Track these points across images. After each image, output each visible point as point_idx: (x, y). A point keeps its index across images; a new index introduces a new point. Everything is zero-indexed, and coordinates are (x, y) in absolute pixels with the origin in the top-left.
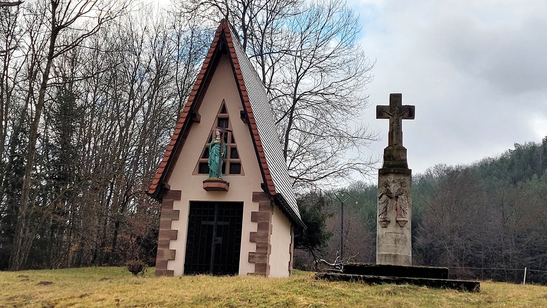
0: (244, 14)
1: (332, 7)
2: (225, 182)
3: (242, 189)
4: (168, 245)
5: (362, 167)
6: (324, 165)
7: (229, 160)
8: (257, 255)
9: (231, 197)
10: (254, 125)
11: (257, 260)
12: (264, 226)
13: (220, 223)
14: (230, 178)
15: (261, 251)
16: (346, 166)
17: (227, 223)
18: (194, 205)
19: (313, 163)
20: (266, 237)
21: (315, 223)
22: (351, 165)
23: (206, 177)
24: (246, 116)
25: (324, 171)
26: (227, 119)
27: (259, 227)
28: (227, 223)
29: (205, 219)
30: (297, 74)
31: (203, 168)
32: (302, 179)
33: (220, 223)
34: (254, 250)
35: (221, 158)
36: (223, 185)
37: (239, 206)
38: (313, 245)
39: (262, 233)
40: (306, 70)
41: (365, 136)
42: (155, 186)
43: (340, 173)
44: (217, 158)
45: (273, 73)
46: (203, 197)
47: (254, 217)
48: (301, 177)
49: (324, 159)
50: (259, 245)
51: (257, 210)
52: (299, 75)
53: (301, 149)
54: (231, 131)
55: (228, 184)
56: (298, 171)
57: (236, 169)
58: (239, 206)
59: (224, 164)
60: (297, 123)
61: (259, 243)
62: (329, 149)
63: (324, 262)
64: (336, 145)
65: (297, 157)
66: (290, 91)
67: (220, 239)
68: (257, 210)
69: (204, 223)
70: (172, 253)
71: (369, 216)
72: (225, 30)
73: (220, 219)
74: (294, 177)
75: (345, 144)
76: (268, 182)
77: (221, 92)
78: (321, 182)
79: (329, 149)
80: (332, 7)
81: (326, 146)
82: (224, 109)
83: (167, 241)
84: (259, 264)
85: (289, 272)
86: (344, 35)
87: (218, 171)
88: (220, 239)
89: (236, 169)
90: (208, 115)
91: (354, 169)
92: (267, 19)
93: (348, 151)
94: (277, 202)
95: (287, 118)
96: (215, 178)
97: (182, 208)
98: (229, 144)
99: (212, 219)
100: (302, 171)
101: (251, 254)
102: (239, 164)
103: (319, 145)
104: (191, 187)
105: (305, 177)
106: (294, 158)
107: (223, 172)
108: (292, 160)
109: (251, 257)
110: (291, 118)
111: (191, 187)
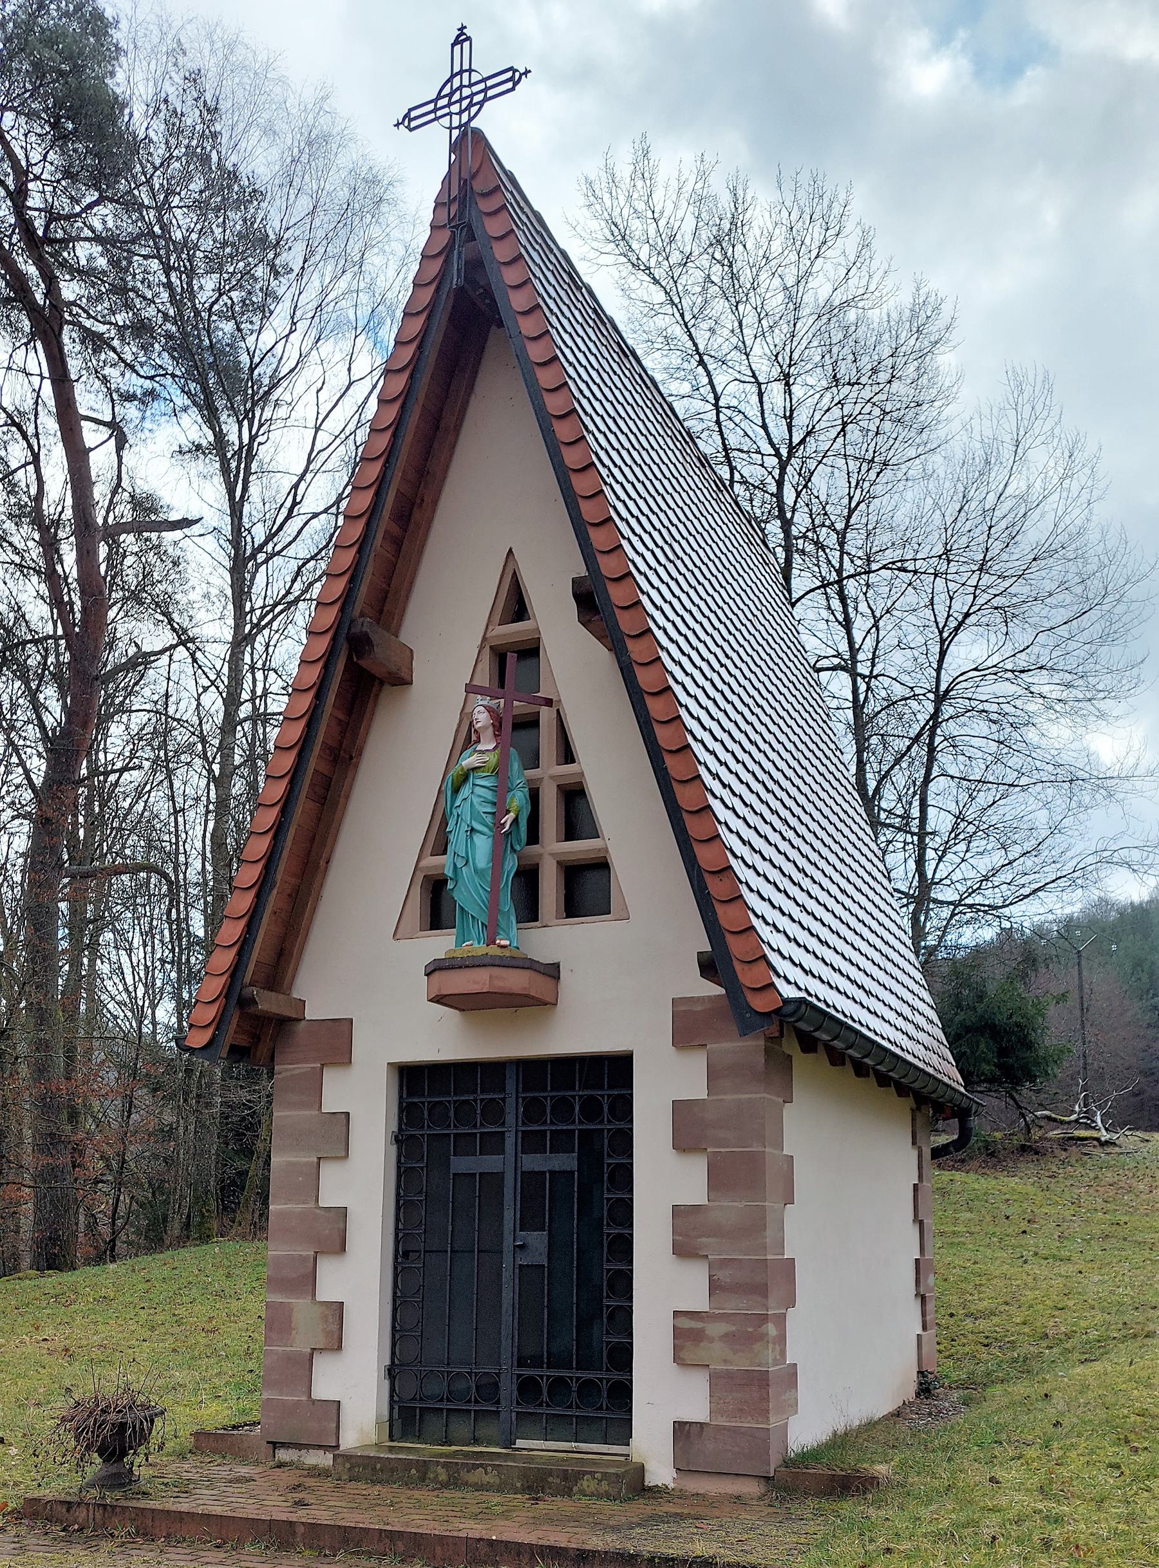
0: (780, 484)
1: (1022, 433)
2: (530, 965)
3: (616, 987)
4: (309, 1281)
5: (1136, 855)
6: (1029, 862)
7: (554, 848)
8: (716, 1329)
9: (572, 1034)
10: (646, 641)
11: (716, 1353)
12: (745, 1172)
13: (533, 1162)
14: (557, 939)
15: (733, 1305)
16: (1091, 859)
17: (567, 1162)
18: (413, 1079)
19: (998, 858)
20: (758, 1227)
21: (1018, 1025)
22: (1105, 854)
23: (441, 944)
24: (599, 603)
25: (1032, 877)
26: (530, 651)
27: (717, 1180)
28: (567, 1162)
29: (464, 1144)
30: (941, 633)
31: (436, 903)
32: (970, 906)
33: (533, 1162)
34: (700, 1302)
35: (502, 841)
36: (515, 981)
37: (617, 1068)
38: (1016, 1082)
39: (732, 1208)
40: (963, 622)
41: (1141, 771)
42: (211, 1013)
43: (1073, 878)
44: (483, 845)
45: (878, 642)
46: (442, 1039)
47: (689, 1128)
48: (969, 901)
49: (1028, 846)
50: (724, 1275)
51: (696, 1088)
52: (945, 635)
53: (962, 825)
54: (549, 702)
55: (553, 972)
56: (958, 885)
57: (587, 889)
58: (617, 1068)
59: (528, 877)
60: (944, 758)
61: (724, 1263)
62: (1041, 818)
63: (1049, 1118)
64: (1060, 804)
65: (954, 849)
66: (925, 681)
67: (537, 1240)
68: (696, 1088)
69: (461, 1164)
70: (325, 1319)
71: (1134, 968)
72: (479, 186)
73: (531, 1143)
74: (949, 903)
75: (1087, 799)
76: (736, 946)
77: (495, 523)
78: (1023, 908)
79: (1041, 818)
80: (1022, 433)
81: (1028, 809)
82: (516, 606)
83: (304, 1259)
84: (729, 1375)
85: (916, 1306)
86: (1060, 513)
87: (493, 906)
88: (537, 1240)
89: (587, 889)
90: (444, 641)
91: (1117, 863)
92: (851, 499)
93: (1096, 814)
94: (809, 1039)
95: (920, 752)
96: (476, 947)
97: (362, 1097)
98: (550, 771)
99: (493, 1144)
100: (969, 883)
101: (686, 1323)
102: (602, 866)
103: (1013, 807)
104: (382, 999)
105: (977, 899)
106: (944, 852)
107: (529, 911)
108: (940, 859)
109: (687, 1335)
110: (932, 750)
111: (382, 999)
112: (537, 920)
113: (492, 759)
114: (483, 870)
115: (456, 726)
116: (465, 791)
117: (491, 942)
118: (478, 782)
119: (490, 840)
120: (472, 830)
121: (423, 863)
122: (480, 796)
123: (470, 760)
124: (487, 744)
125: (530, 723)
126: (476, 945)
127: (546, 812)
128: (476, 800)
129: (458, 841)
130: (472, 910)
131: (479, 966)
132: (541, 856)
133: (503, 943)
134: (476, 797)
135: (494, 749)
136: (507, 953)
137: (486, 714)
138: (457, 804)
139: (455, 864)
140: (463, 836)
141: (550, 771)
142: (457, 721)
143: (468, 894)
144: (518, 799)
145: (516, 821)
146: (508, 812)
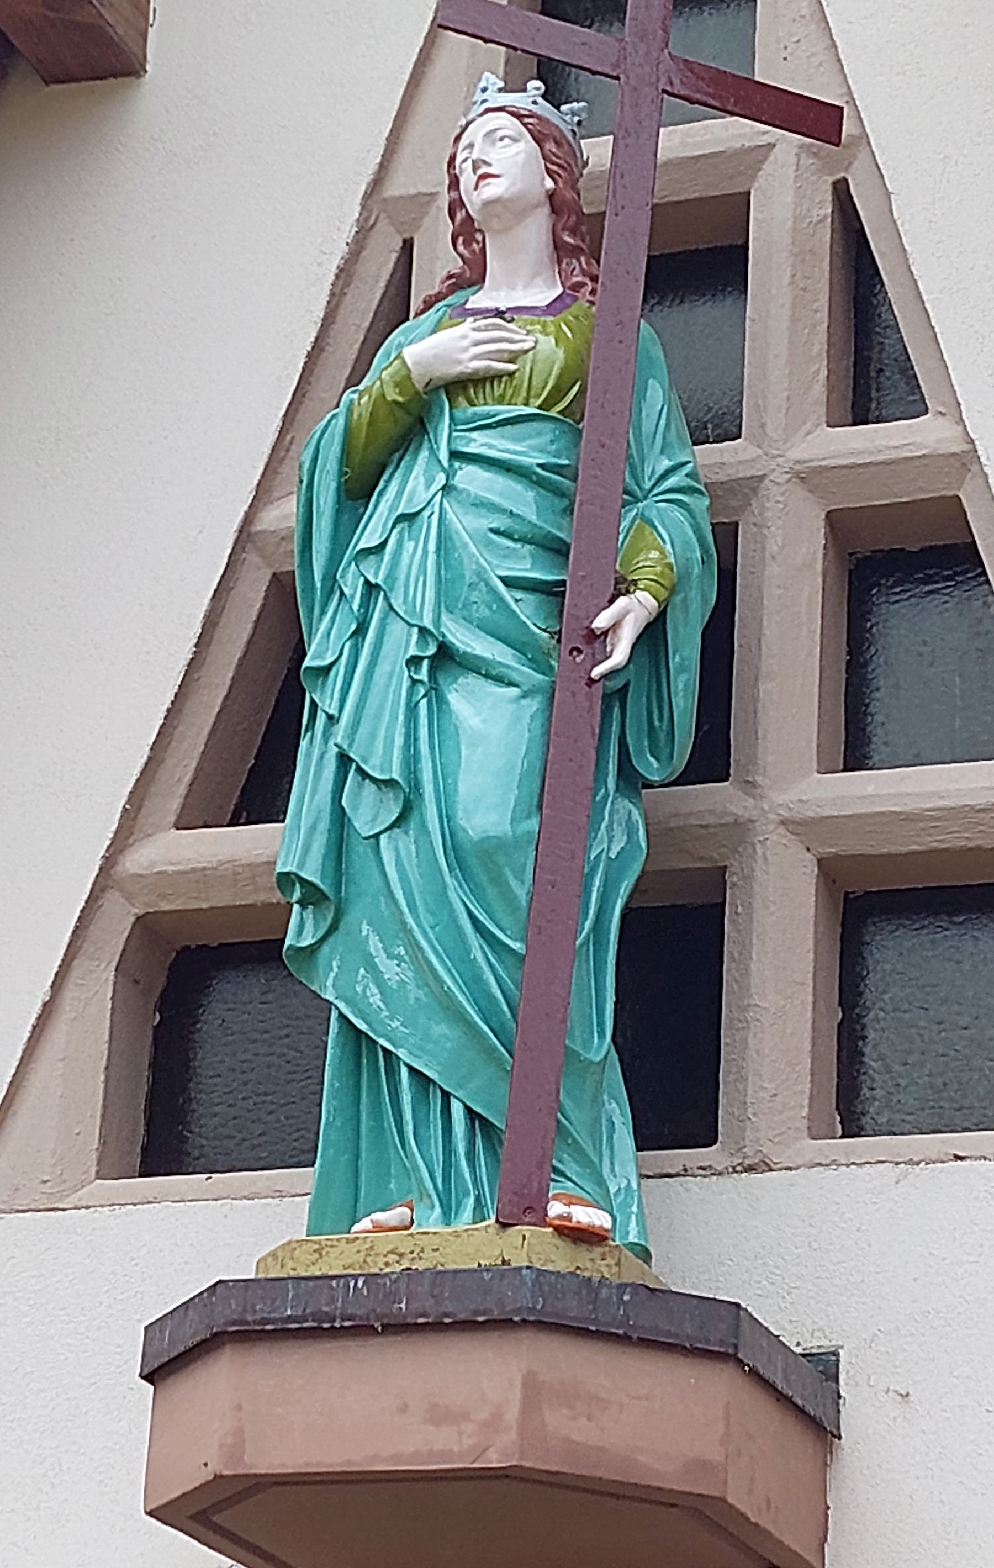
2: (713, 1336)
23: (234, 1227)
44: (493, 729)
55: (805, 1398)
87: (526, 1038)
107: (677, 1095)
112: (710, 1139)
113: (546, 350)
114: (491, 849)
115: (340, 251)
116: (411, 483)
117: (522, 1207)
118: (478, 443)
119: (534, 705)
120: (445, 658)
121: (143, 858)
122: (481, 505)
123: (433, 347)
124: (522, 279)
125: (700, 261)
126: (431, 1220)
127: (771, 630)
128: (465, 524)
129: (360, 703)
130: (421, 1044)
131: (468, 1326)
132: (739, 831)
133: (584, 1216)
134: (458, 517)
135: (553, 308)
136: (592, 1264)
137: (527, 145)
138: (369, 539)
139: (340, 818)
140: (392, 680)
141: (798, 441)
142: (348, 231)
143: (391, 974)
144: (667, 537)
145: (653, 635)
146: (623, 586)
